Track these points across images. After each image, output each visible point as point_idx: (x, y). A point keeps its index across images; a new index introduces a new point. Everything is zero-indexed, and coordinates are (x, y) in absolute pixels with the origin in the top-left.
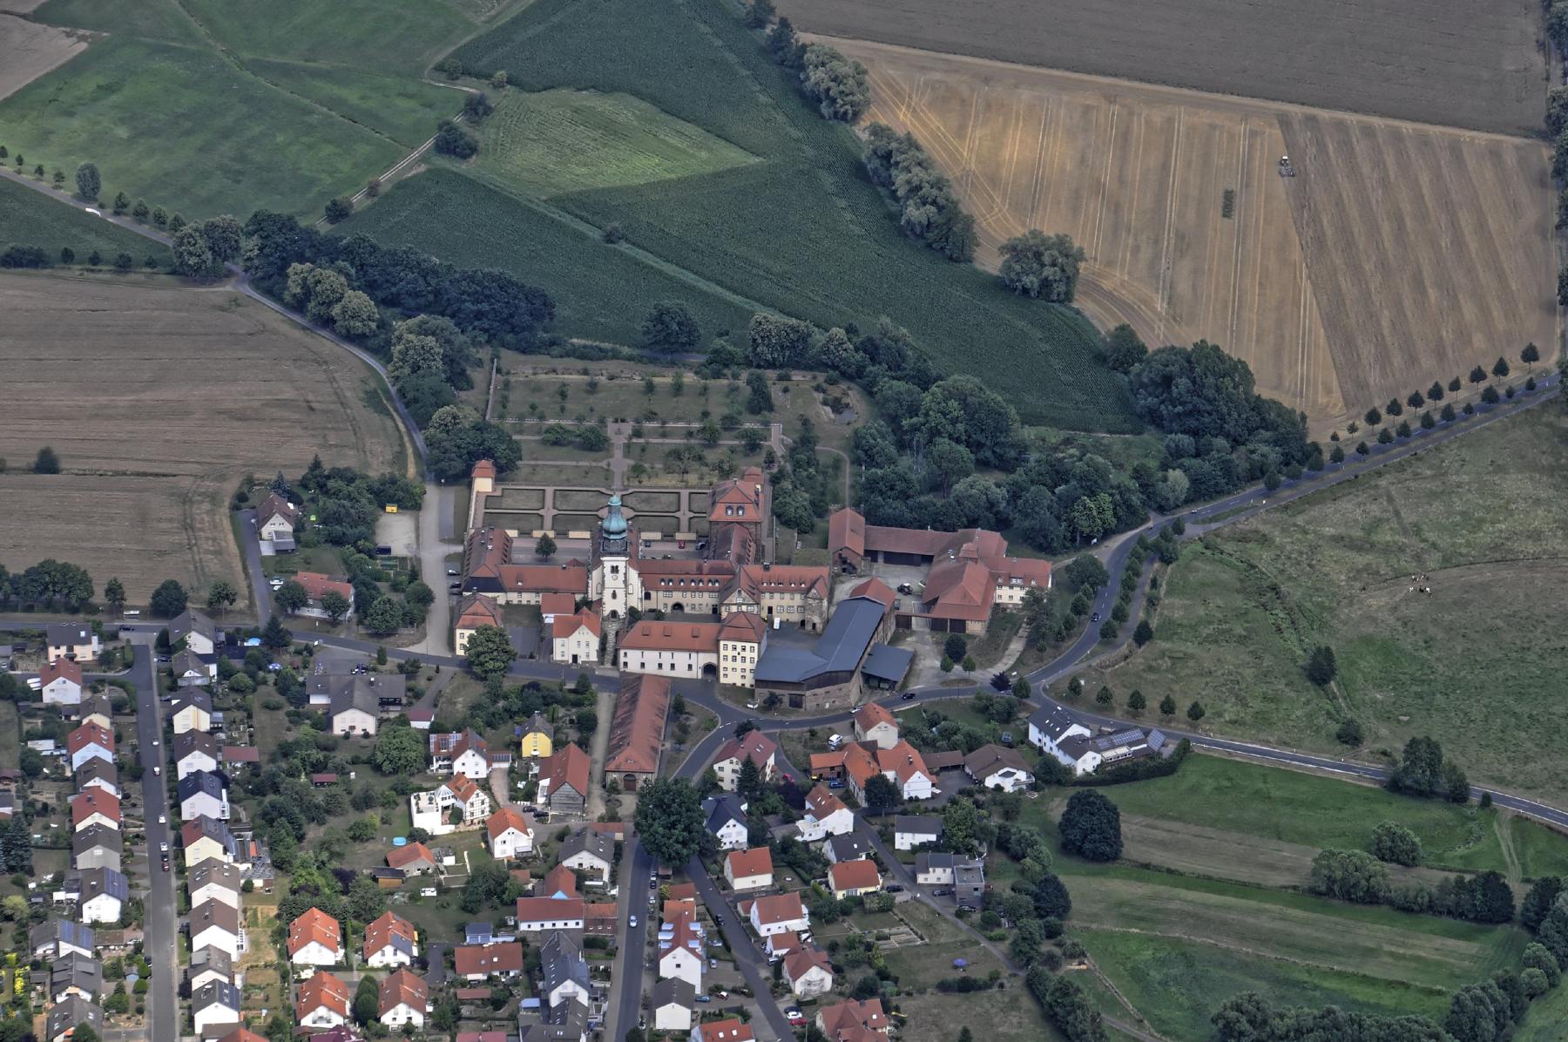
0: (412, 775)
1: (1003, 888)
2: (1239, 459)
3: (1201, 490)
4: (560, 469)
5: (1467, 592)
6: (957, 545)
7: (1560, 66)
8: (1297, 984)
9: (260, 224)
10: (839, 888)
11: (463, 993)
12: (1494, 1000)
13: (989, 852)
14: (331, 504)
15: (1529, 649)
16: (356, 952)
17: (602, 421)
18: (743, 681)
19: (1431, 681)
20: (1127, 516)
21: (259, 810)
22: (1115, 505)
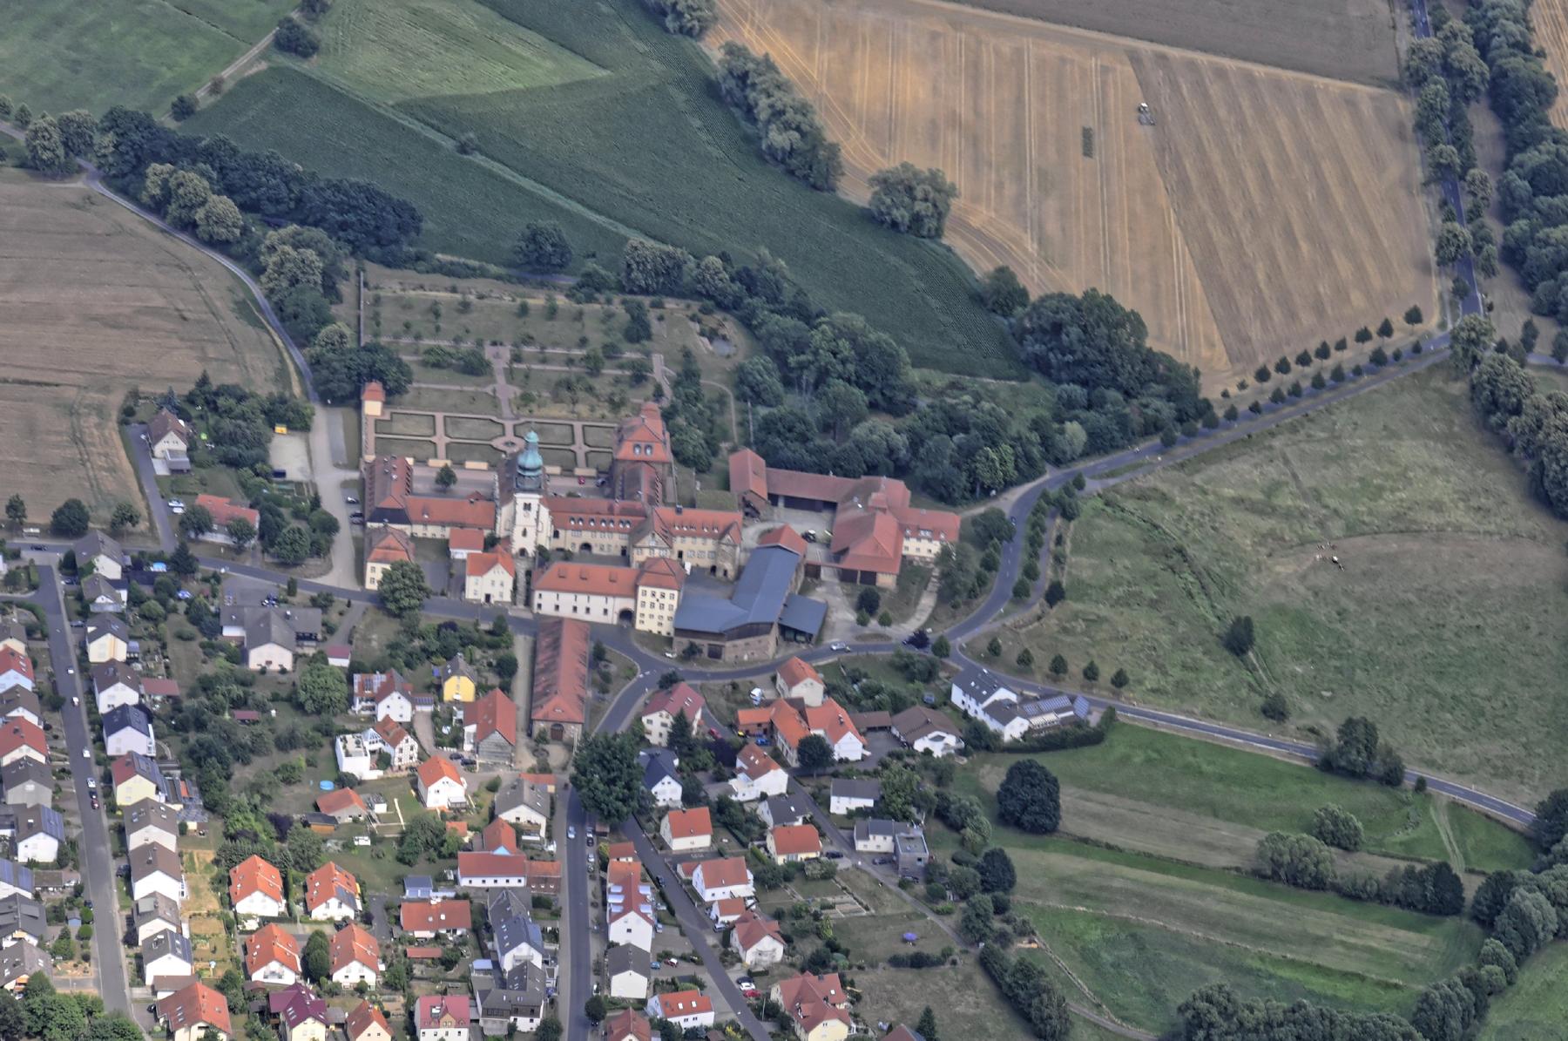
0: (335, 715)
1: (944, 857)
2: (1131, 410)
3: (1098, 444)
4: (445, 393)
5: (1374, 563)
6: (865, 494)
7: (1406, 15)
8: (1249, 971)
9: (114, 120)
10: (780, 852)
11: (412, 951)
12: (1461, 999)
13: (926, 821)
14: (227, 424)
15: (1444, 626)
16: (297, 903)
17: (480, 343)
18: (660, 629)
20: (1028, 469)
21: (185, 747)
22: (1017, 457)
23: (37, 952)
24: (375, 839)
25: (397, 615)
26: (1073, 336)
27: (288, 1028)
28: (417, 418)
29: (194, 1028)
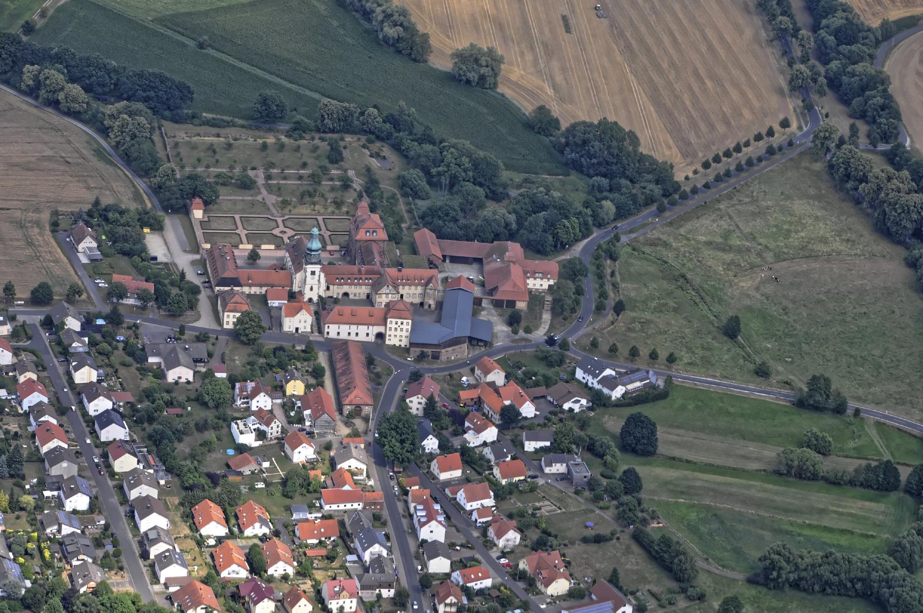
3: (622, 213)
4: (235, 202)
8: (787, 532)
16: (234, 526)
17: (245, 169)
18: (400, 343)
19: (796, 335)
23: (94, 567)
25: (250, 342)
26: (597, 148)
27: (252, 605)
28: (224, 219)
29: (199, 609)
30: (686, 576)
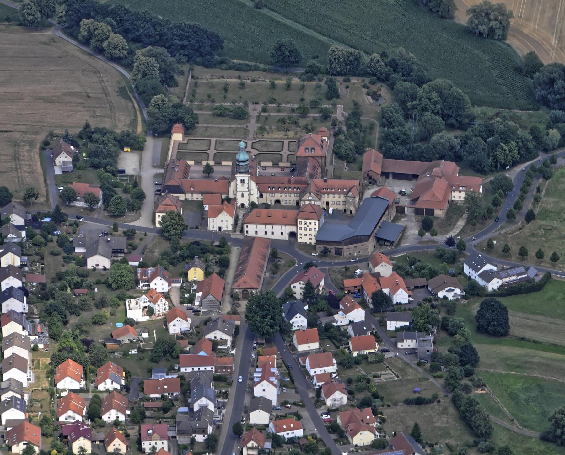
0: (128, 290)
4: (221, 129)
17: (246, 104)
22: (519, 148)
24: (140, 350)
29: (21, 444)
30: (479, 431)
